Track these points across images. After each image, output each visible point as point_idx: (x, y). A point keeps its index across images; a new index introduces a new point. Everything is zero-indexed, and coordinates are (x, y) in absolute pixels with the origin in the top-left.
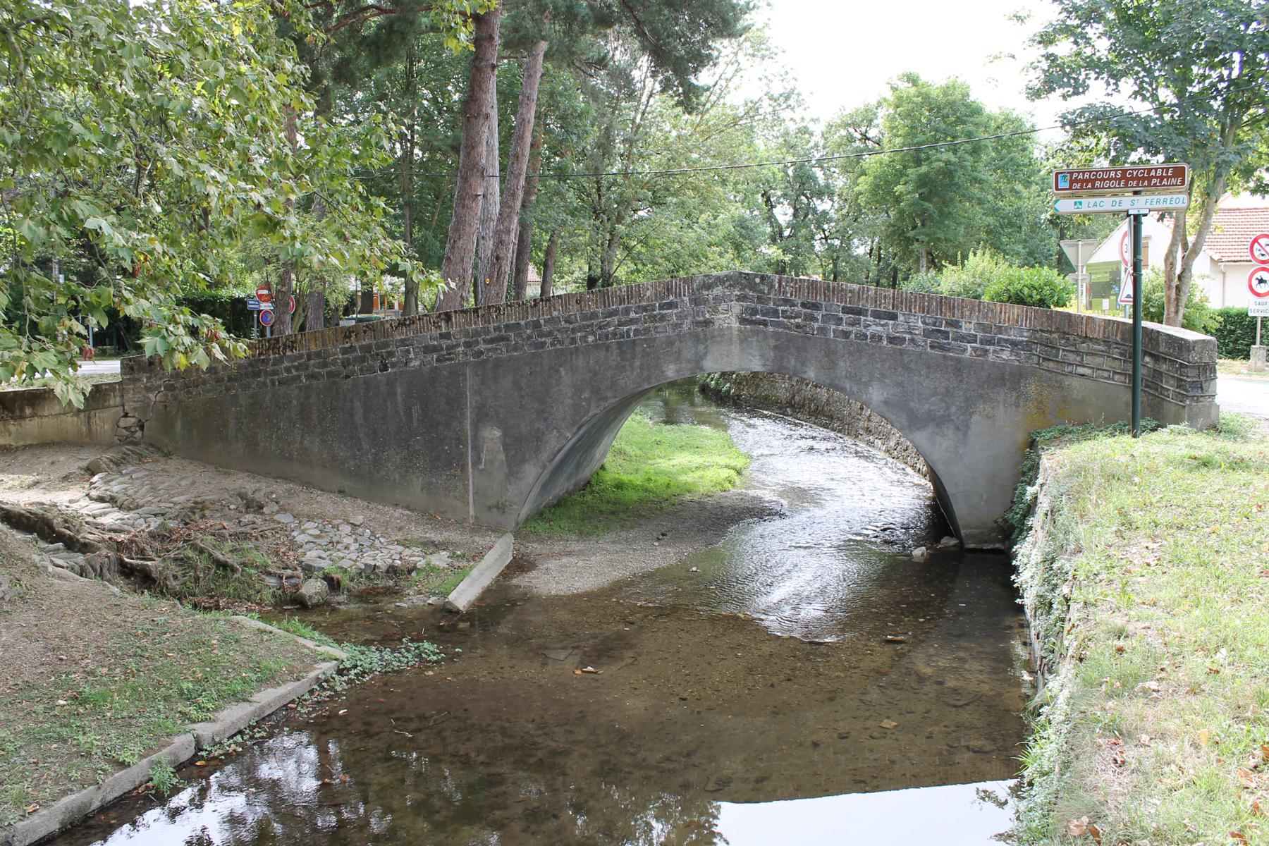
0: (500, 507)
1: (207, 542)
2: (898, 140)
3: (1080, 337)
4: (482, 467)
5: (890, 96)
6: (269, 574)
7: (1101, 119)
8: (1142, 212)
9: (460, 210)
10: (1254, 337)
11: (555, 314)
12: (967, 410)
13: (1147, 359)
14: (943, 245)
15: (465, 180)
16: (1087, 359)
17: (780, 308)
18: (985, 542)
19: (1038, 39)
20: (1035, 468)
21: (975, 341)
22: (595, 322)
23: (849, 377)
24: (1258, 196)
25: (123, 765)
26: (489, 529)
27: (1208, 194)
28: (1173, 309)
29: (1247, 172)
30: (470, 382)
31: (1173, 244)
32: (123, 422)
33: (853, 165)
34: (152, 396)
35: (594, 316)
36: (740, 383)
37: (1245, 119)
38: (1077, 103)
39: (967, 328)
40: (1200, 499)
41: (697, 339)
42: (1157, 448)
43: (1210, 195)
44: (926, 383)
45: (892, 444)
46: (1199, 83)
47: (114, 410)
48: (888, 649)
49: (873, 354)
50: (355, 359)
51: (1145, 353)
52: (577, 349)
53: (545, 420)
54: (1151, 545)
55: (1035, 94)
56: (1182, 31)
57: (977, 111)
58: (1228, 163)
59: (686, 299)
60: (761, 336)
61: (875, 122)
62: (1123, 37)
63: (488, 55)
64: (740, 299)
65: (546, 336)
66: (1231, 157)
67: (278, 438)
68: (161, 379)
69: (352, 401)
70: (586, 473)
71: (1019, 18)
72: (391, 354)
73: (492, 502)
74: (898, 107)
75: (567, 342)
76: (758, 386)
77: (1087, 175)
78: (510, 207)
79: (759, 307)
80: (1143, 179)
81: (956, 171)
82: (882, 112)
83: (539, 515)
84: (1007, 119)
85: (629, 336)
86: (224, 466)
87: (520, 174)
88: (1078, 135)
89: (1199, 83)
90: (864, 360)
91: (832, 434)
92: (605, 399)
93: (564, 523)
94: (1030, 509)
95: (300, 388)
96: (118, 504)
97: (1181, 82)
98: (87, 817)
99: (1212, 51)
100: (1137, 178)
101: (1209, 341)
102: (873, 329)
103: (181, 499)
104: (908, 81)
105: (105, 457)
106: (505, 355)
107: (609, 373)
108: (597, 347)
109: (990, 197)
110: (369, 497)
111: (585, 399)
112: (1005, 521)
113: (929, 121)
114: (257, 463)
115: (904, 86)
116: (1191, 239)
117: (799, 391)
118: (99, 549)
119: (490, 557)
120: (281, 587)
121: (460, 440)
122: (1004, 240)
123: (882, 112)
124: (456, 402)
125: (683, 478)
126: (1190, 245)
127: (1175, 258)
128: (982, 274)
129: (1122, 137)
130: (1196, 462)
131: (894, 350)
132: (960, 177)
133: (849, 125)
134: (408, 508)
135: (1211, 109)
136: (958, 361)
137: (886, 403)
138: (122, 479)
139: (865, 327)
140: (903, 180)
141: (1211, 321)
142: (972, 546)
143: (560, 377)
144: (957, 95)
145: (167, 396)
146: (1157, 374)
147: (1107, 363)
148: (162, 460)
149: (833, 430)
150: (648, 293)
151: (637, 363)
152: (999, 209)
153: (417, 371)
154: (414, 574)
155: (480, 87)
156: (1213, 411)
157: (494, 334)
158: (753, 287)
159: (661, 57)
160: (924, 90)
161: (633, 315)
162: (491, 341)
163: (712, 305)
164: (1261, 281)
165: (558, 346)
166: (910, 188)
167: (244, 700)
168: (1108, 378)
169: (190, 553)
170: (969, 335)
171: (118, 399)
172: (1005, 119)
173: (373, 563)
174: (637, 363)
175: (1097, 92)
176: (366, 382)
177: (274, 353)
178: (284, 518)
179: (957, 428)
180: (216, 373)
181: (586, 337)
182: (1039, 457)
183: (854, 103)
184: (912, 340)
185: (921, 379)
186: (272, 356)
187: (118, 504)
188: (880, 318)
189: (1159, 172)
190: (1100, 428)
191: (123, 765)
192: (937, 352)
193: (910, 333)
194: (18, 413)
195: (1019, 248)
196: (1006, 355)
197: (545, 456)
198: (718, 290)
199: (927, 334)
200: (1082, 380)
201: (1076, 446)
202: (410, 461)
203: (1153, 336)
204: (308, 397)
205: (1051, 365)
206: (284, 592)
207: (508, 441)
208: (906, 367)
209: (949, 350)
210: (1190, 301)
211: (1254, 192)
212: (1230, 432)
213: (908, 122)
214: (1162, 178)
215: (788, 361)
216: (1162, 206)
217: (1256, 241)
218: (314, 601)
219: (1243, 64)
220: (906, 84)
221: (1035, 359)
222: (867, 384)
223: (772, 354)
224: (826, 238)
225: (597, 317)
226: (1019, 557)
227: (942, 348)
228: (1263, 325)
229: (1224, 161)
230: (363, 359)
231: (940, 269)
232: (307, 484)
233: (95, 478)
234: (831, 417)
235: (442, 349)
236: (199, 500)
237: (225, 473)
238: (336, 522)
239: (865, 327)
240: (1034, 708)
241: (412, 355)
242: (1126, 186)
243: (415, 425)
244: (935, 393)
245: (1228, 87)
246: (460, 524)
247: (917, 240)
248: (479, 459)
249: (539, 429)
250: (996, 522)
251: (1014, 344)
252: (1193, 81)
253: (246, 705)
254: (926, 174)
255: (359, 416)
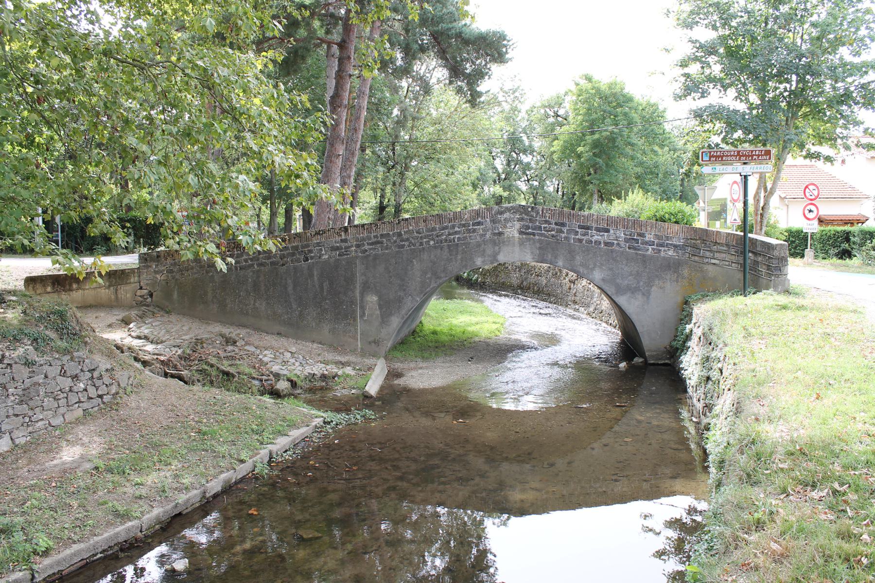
0: (376, 342)
1: (213, 361)
2: (580, 118)
3: (713, 242)
4: (365, 318)
5: (574, 88)
6: (254, 378)
7: (716, 114)
8: (748, 174)
9: (328, 164)
10: (807, 245)
11: (411, 228)
12: (649, 284)
13: (750, 254)
14: (609, 186)
15: (332, 145)
16: (717, 255)
17: (543, 226)
18: (660, 359)
19: (680, 64)
20: (690, 315)
21: (654, 245)
22: (434, 233)
23: (582, 265)
24: (808, 160)
25: (242, 461)
26: (370, 355)
27: (779, 159)
28: (759, 228)
29: (802, 146)
30: (359, 268)
31: (759, 188)
32: (139, 293)
33: (549, 133)
34: (158, 276)
35: (434, 229)
36: (485, 275)
37: (800, 114)
38: (703, 103)
39: (649, 237)
40: (783, 323)
41: (494, 243)
42: (758, 302)
43: (780, 159)
44: (626, 269)
45: (591, 309)
46: (773, 91)
47: (133, 285)
48: (618, 409)
49: (596, 252)
50: (288, 254)
51: (750, 251)
52: (423, 249)
53: (404, 290)
54: (761, 342)
55: (678, 98)
56: (764, 61)
57: (630, 100)
58: (791, 140)
59: (488, 220)
60: (532, 241)
61: (564, 105)
62: (729, 64)
63: (348, 69)
64: (519, 220)
65: (405, 241)
66: (793, 137)
67: (239, 302)
68: (164, 266)
69: (286, 279)
70: (414, 326)
71: (667, 50)
72: (310, 251)
73: (371, 339)
74: (579, 96)
75: (417, 244)
76: (497, 276)
77: (719, 153)
78: (350, 161)
79: (530, 225)
80: (749, 156)
81: (617, 138)
82: (568, 99)
83: (394, 348)
84: (648, 104)
85: (454, 241)
86: (205, 319)
87: (357, 141)
88: (702, 122)
89: (773, 91)
90: (591, 256)
91: (550, 305)
92: (440, 278)
93: (412, 353)
94: (688, 337)
95: (254, 272)
96: (150, 340)
97: (762, 91)
98: (230, 487)
99: (780, 74)
100: (745, 155)
101: (784, 245)
102: (596, 238)
103: (187, 337)
104: (586, 79)
105: (133, 313)
106: (380, 252)
107: (443, 263)
108: (435, 247)
109: (639, 155)
110: (297, 337)
111: (428, 278)
112: (671, 347)
113: (600, 106)
114: (224, 315)
115: (584, 83)
116: (769, 186)
117: (526, 279)
118: (153, 364)
119: (377, 369)
120: (263, 385)
121: (353, 302)
122: (647, 182)
123: (568, 99)
124: (350, 280)
125: (470, 329)
126: (769, 189)
127: (759, 197)
128: (637, 205)
129: (728, 124)
130: (779, 307)
131: (608, 250)
132: (619, 142)
133: (546, 107)
134: (320, 343)
135: (780, 108)
136: (644, 256)
137: (603, 280)
138: (146, 326)
139: (591, 236)
140: (582, 144)
141: (781, 235)
142: (652, 362)
143: (413, 265)
144: (617, 89)
145: (168, 276)
146: (756, 263)
147: (728, 257)
148: (166, 315)
149: (551, 302)
150: (466, 216)
151: (459, 257)
152: (644, 162)
153: (326, 262)
154: (336, 379)
155: (342, 88)
156: (786, 282)
157: (374, 240)
158: (527, 213)
159: (456, 71)
160: (596, 85)
161: (457, 229)
162: (372, 244)
163: (503, 223)
164: (810, 211)
165: (412, 247)
166: (587, 149)
167: (285, 435)
168: (729, 265)
169: (206, 367)
170: (650, 241)
171: (136, 278)
172: (647, 104)
173: (313, 372)
174: (459, 257)
175: (716, 97)
176: (295, 268)
177: (237, 251)
178: (252, 349)
179: (643, 294)
180: (200, 262)
181: (429, 241)
182: (692, 309)
183: (549, 93)
184: (618, 244)
185: (623, 266)
186: (236, 252)
187: (150, 340)
188: (600, 232)
189: (757, 152)
190: (726, 292)
191: (242, 461)
192: (632, 251)
193: (617, 240)
194: (68, 287)
195: (656, 188)
196: (671, 253)
197: (403, 312)
198: (507, 215)
199: (626, 240)
200: (714, 267)
201: (712, 302)
202: (322, 315)
203: (754, 242)
204: (258, 277)
205: (696, 258)
206: (264, 388)
207: (381, 303)
208: (614, 260)
209: (639, 250)
210: (768, 223)
211: (805, 157)
212: (796, 294)
213: (586, 106)
214: (759, 156)
215: (547, 256)
216: (762, 170)
217: (807, 187)
218: (285, 393)
219: (798, 82)
220: (585, 81)
221: (687, 254)
222: (593, 269)
223: (538, 252)
224: (528, 180)
225: (436, 230)
226: (684, 363)
227: (635, 248)
228: (812, 238)
229: (789, 139)
230: (293, 254)
231: (610, 202)
232: (258, 329)
233: (131, 325)
234: (549, 295)
235: (342, 249)
236: (199, 337)
237: (206, 323)
238: (281, 351)
239: (591, 236)
240: (705, 427)
241: (323, 252)
242: (740, 160)
243: (325, 293)
244: (631, 275)
245: (789, 95)
246: (353, 352)
247: (592, 183)
248: (364, 314)
249: (400, 296)
250: (666, 348)
251: (675, 246)
252: (769, 90)
253: (287, 437)
254: (598, 140)
255: (290, 289)
